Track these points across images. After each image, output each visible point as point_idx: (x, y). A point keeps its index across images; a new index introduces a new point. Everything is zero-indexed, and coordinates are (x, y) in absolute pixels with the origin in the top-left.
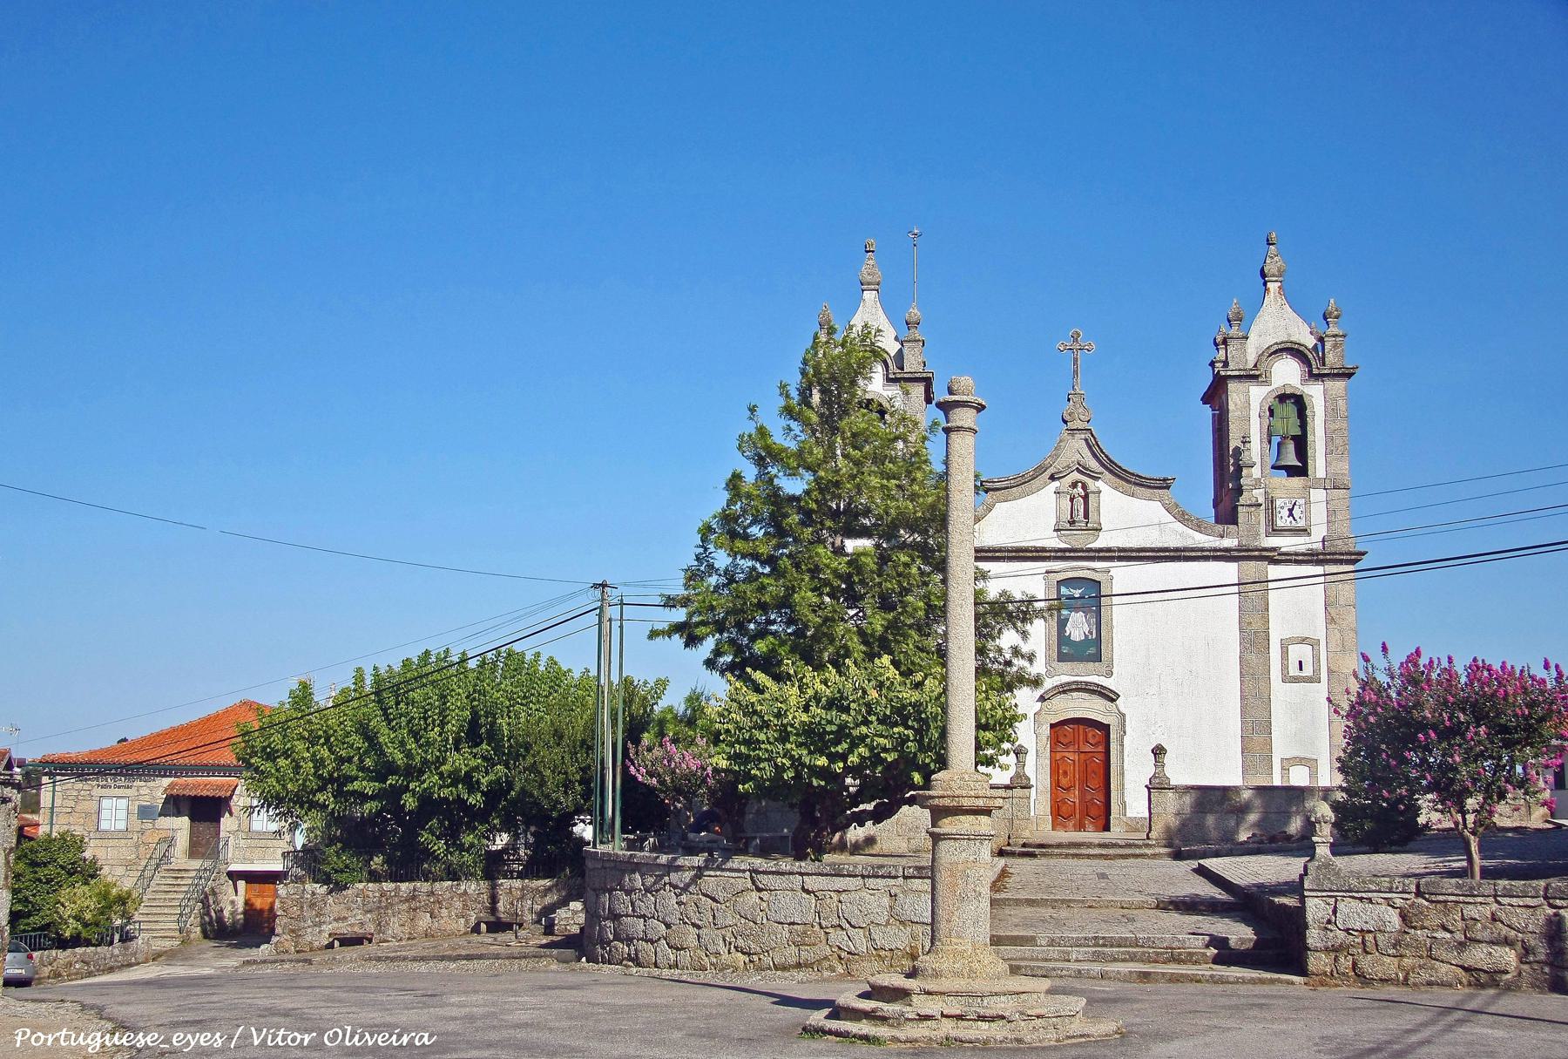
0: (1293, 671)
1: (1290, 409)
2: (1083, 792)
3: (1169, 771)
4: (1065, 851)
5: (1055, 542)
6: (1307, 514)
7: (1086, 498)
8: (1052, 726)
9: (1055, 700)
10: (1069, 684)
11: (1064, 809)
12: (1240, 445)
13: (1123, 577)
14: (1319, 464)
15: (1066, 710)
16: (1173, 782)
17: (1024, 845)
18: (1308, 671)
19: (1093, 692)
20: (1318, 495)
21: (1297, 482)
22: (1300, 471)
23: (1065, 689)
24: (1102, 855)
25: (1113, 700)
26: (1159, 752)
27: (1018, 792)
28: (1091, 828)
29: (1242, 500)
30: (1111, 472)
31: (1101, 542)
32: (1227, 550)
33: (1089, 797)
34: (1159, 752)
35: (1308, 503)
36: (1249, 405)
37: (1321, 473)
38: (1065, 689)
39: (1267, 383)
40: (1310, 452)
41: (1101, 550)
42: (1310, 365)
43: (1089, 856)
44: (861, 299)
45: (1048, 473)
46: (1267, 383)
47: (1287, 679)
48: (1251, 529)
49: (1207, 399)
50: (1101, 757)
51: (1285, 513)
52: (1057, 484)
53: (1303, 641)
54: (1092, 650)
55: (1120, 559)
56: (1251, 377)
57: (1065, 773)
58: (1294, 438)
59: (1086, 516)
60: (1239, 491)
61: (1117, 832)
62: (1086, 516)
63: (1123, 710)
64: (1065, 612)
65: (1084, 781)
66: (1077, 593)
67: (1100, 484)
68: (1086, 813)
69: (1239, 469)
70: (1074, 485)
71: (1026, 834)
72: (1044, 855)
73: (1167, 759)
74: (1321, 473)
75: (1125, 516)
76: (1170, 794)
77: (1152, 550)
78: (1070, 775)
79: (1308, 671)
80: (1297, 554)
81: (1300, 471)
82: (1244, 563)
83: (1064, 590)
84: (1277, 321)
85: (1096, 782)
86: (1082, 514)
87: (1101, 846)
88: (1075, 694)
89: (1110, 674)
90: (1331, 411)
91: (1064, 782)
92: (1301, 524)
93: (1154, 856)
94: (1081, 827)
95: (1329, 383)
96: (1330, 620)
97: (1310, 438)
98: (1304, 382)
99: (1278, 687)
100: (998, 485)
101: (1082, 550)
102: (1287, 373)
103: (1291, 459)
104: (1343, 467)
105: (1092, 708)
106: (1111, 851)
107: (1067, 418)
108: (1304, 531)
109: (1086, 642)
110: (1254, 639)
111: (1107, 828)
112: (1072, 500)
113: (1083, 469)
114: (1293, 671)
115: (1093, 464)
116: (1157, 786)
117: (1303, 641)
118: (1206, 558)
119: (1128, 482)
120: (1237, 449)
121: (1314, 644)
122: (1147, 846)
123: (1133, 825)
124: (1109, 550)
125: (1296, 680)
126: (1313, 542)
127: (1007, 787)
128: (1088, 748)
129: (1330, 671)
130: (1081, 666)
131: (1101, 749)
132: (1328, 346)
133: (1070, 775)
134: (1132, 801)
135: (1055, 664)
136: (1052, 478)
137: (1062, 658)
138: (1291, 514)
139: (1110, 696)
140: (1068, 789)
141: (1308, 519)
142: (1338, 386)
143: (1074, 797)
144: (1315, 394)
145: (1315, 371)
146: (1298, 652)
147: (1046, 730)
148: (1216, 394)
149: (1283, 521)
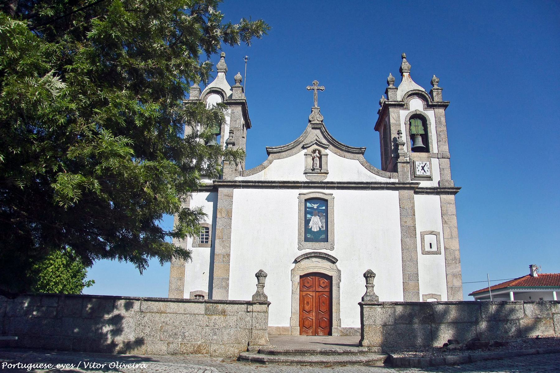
0: (427, 248)
1: (419, 122)
2: (317, 314)
3: (376, 291)
4: (291, 358)
5: (303, 178)
6: (430, 168)
7: (320, 158)
8: (301, 277)
9: (303, 263)
10: (310, 253)
11: (306, 323)
12: (397, 136)
13: (339, 197)
14: (434, 147)
15: (308, 268)
16: (381, 300)
17: (259, 352)
18: (434, 249)
19: (323, 258)
20: (435, 161)
21: (424, 155)
22: (426, 149)
23: (307, 257)
24: (322, 363)
25: (334, 263)
26: (369, 276)
27: (257, 307)
28: (321, 333)
29: (399, 160)
30: (333, 145)
31: (329, 179)
32: (393, 183)
33: (320, 317)
34: (369, 276)
35: (430, 164)
36: (399, 119)
37: (435, 151)
38: (307, 257)
39: (407, 109)
40: (430, 141)
41: (328, 183)
42: (427, 101)
43: (311, 363)
44: (216, 75)
45: (301, 145)
46: (407, 109)
47: (424, 253)
48: (403, 174)
49: (377, 128)
50: (327, 294)
51: (420, 168)
52: (305, 151)
53: (432, 233)
54: (323, 236)
55: (338, 188)
56: (400, 105)
57: (308, 303)
58: (421, 135)
59: (321, 166)
60: (398, 156)
61: (336, 336)
62: (321, 166)
63: (339, 268)
64: (309, 216)
65: (318, 308)
66: (315, 206)
67: (327, 151)
68: (319, 325)
69: (397, 146)
70: (314, 152)
71: (262, 341)
72: (271, 362)
73: (375, 281)
74: (435, 151)
75: (341, 167)
76: (379, 309)
77: (355, 183)
78: (310, 304)
79: (434, 249)
80: (427, 188)
81: (426, 149)
82: (403, 192)
83: (308, 205)
84: (408, 85)
85: (324, 308)
86: (318, 165)
87: (323, 353)
88: (314, 259)
89: (332, 249)
90: (438, 122)
91: (307, 308)
92: (428, 174)
93: (368, 364)
94: (316, 333)
95: (437, 110)
96: (444, 222)
97: (429, 134)
98: (425, 109)
99: (421, 258)
100: (275, 150)
101: (318, 183)
102: (416, 105)
103: (420, 143)
104: (445, 148)
105: (322, 267)
106: (331, 359)
107: (311, 119)
108: (429, 178)
109: (320, 232)
110: (408, 231)
111: (330, 334)
112: (313, 159)
113: (319, 143)
114: (427, 248)
115: (324, 141)
116: (367, 303)
117: (432, 233)
118: (382, 188)
119: (342, 150)
120: (395, 138)
121: (437, 234)
122: (362, 352)
123: (347, 332)
124: (332, 183)
125: (429, 253)
126: (434, 184)
127: (249, 303)
128: (321, 289)
129: (446, 249)
130: (317, 245)
131: (327, 290)
132: (435, 94)
133: (310, 304)
134: (347, 316)
135: (303, 243)
136: (303, 148)
137: (307, 240)
138: (423, 168)
139: (333, 260)
140: (309, 312)
141: (431, 172)
142: (441, 111)
143: (312, 316)
144: (430, 114)
145: (430, 103)
146: (429, 239)
147: (297, 279)
148: (384, 112)
149: (419, 172)
